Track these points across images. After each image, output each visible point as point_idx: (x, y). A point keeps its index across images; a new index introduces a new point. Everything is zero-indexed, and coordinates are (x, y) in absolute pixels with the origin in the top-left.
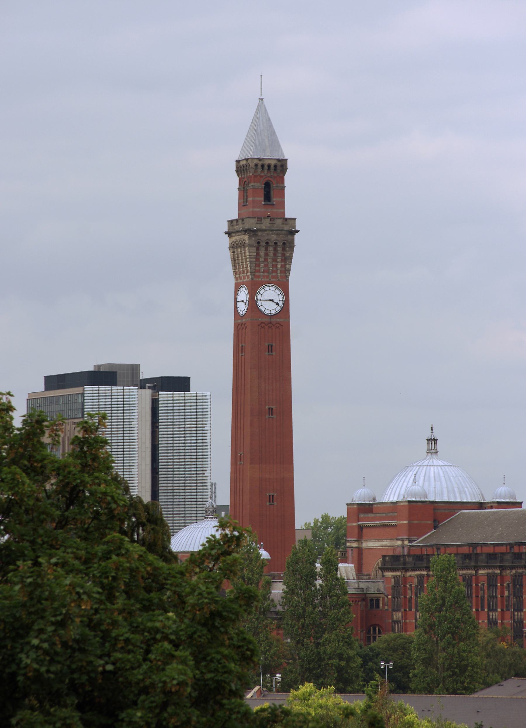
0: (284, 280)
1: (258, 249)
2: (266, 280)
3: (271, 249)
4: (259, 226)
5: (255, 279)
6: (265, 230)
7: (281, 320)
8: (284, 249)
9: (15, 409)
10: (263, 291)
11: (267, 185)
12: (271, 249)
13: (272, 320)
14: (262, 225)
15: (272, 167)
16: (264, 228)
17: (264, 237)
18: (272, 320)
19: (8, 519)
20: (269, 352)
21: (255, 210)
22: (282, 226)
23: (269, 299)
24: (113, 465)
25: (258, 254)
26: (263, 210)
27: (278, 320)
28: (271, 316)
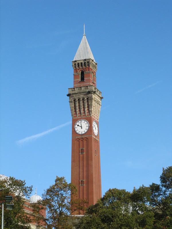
0: (89, 116)
1: (75, 104)
2: (80, 117)
3: (81, 102)
4: (74, 92)
5: (74, 118)
6: (77, 93)
7: (87, 136)
8: (88, 102)
9: (163, 169)
10: (86, 123)
11: (82, 73)
12: (81, 102)
13: (83, 136)
14: (75, 91)
15: (80, 64)
16: (77, 92)
17: (76, 97)
18: (83, 136)
19: (58, 212)
20: (81, 153)
21: (75, 85)
22: (85, 90)
23: (82, 128)
24: (126, 191)
25: (75, 106)
26: (79, 85)
27: (86, 136)
28: (82, 135)
